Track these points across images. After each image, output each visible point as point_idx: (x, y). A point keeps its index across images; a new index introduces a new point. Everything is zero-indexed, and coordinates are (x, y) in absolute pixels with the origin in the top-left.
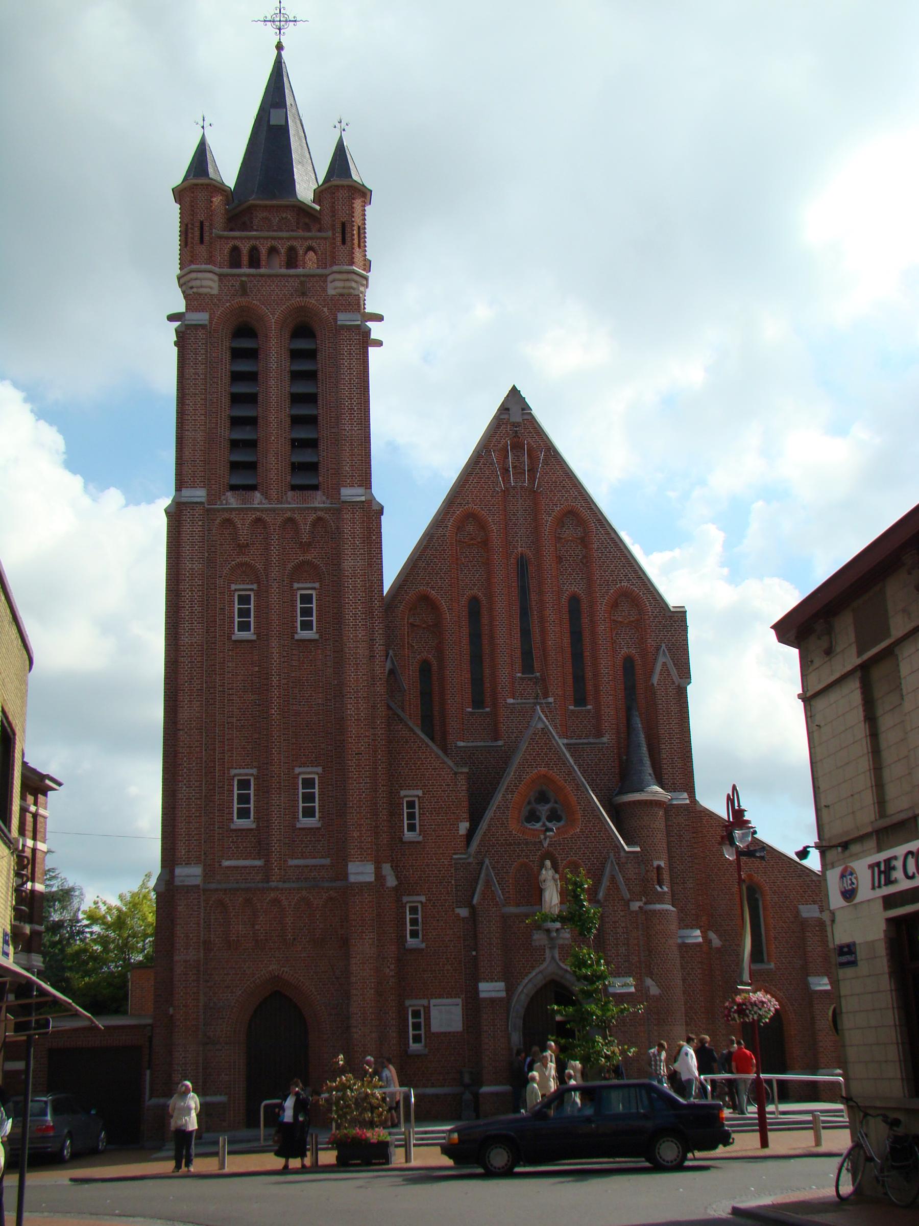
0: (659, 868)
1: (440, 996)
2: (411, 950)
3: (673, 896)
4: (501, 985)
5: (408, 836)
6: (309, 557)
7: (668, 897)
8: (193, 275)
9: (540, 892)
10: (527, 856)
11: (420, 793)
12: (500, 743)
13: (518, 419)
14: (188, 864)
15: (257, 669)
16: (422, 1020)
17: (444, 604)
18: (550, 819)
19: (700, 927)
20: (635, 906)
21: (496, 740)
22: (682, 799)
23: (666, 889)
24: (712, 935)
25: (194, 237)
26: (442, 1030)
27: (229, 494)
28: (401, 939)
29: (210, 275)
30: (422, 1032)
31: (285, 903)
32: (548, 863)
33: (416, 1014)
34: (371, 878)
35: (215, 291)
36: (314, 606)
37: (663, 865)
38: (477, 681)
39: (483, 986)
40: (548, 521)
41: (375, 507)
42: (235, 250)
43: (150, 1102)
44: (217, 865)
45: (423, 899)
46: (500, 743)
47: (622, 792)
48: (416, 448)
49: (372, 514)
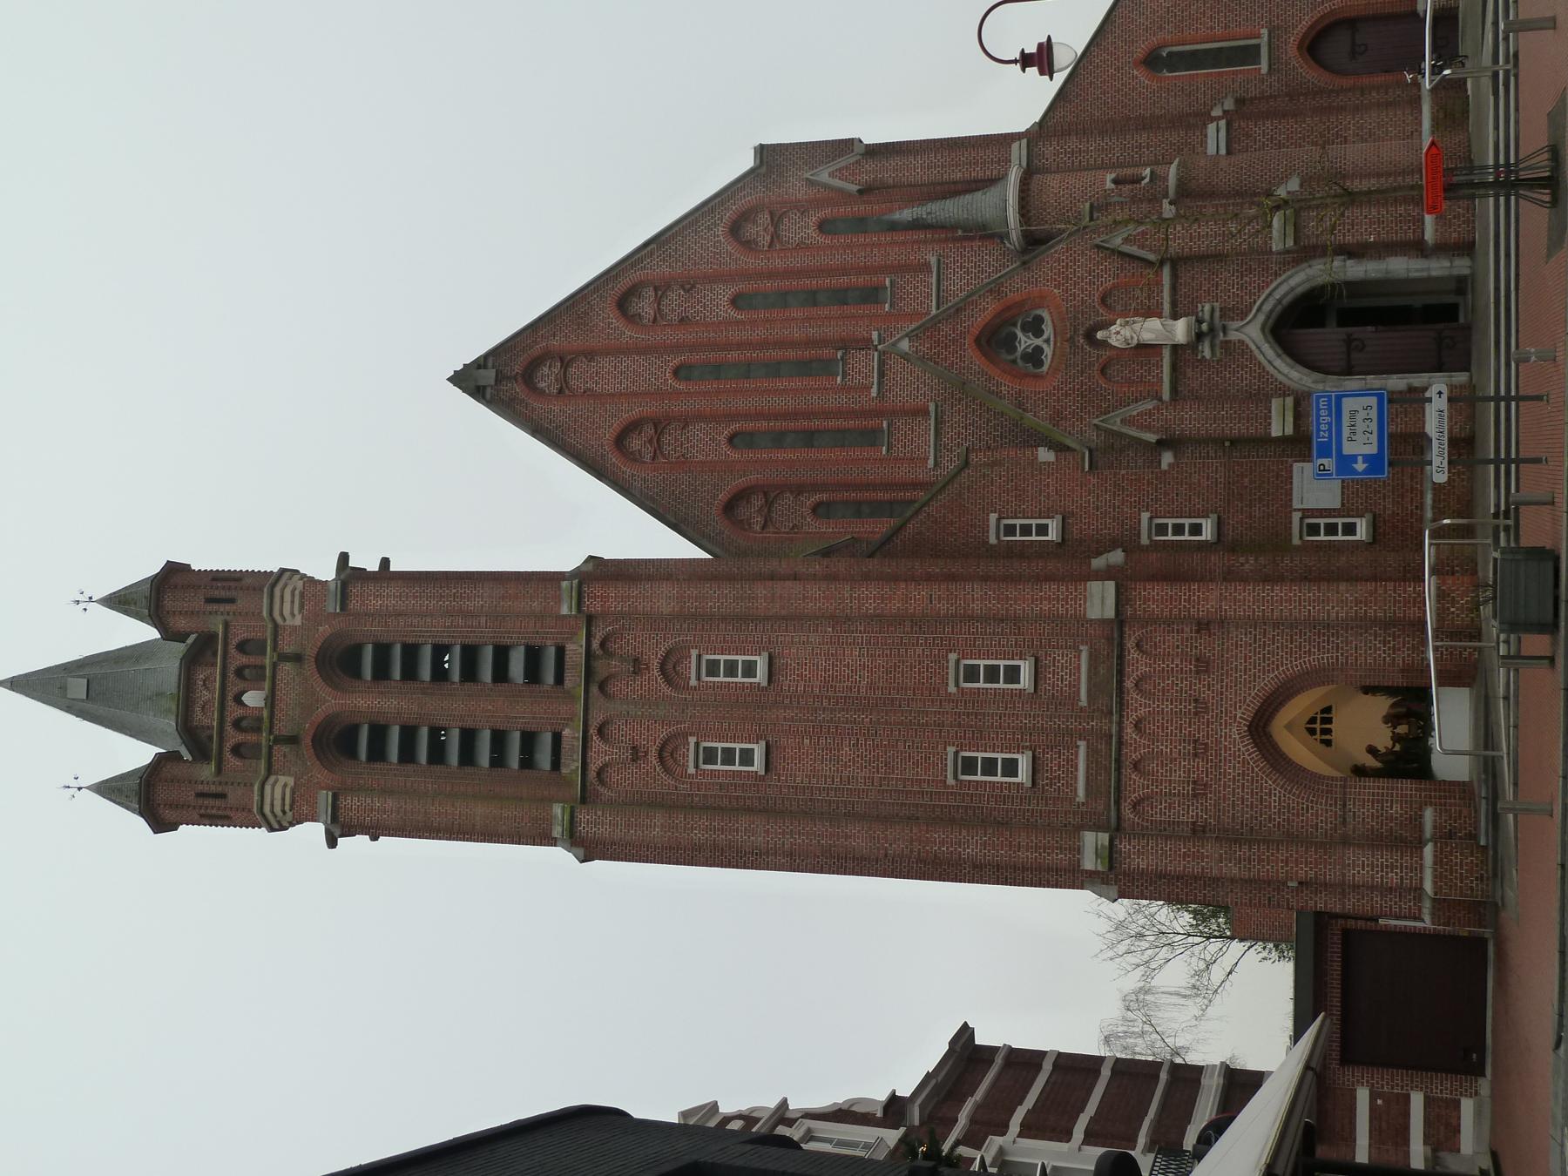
1: (1289, 493)
2: (1219, 535)
3: (1157, 163)
4: (1276, 404)
6: (655, 664)
7: (1159, 170)
8: (267, 809)
9: (1142, 347)
12: (932, 407)
13: (491, 373)
14: (1079, 851)
15: (807, 741)
16: (1322, 521)
17: (742, 482)
18: (1038, 333)
19: (1205, 125)
20: (1168, 210)
21: (927, 413)
22: (1018, 152)
23: (1148, 171)
25: (217, 809)
26: (1374, 438)
27: (564, 771)
28: (1201, 546)
29: (268, 788)
30: (1340, 521)
32: (1100, 335)
33: (1314, 529)
34: (1110, 586)
35: (291, 781)
38: (841, 438)
39: (1276, 432)
40: (629, 334)
41: (590, 567)
42: (237, 750)
43: (1427, 923)
44: (1084, 809)
45: (1145, 516)
46: (932, 407)
47: (1003, 237)
48: (547, 516)
49: (598, 572)
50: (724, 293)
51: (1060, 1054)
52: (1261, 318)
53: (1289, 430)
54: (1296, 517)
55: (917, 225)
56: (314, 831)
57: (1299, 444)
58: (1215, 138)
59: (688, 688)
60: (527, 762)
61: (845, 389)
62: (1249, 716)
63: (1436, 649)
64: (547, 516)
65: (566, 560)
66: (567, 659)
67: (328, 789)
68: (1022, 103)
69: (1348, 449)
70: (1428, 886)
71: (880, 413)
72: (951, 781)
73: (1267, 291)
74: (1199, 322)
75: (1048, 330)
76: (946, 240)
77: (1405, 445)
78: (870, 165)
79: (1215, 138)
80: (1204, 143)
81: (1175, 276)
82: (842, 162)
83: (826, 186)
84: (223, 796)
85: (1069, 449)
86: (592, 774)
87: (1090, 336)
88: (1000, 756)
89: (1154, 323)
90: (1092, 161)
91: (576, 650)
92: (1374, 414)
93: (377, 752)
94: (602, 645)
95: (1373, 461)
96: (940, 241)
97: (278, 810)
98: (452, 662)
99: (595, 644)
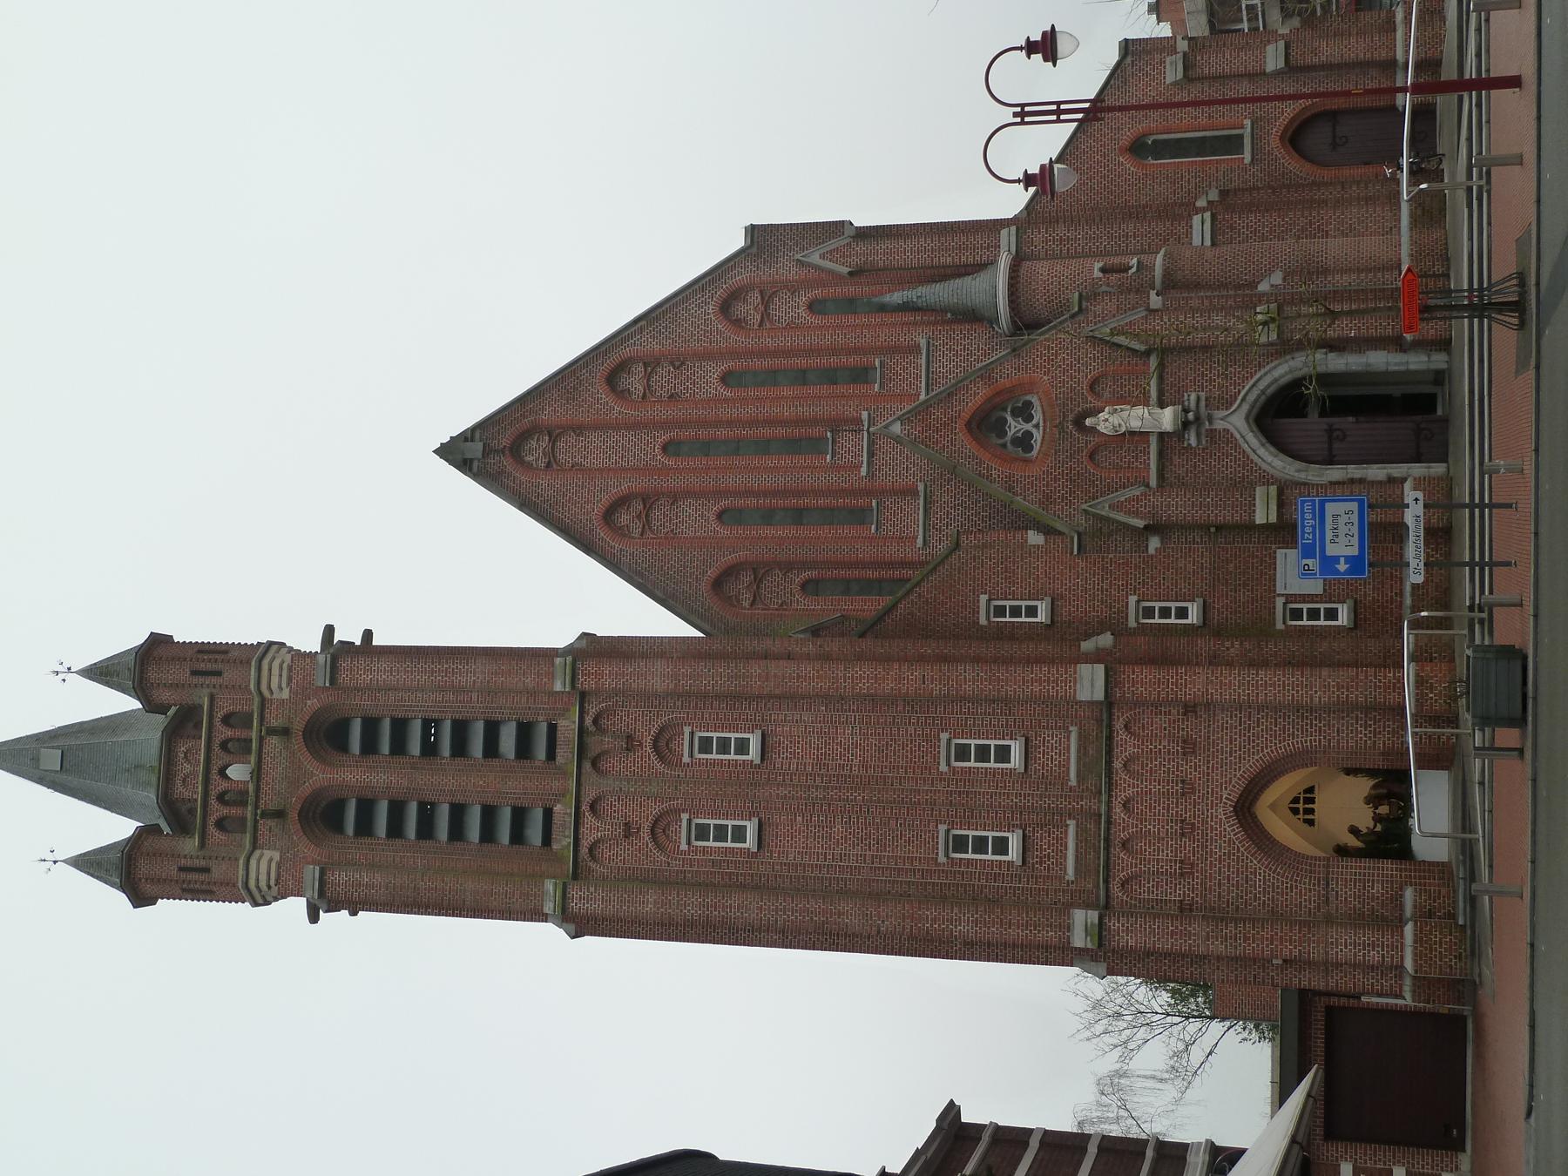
0: (1103, 270)
3: (1143, 252)
4: (1260, 492)
5: (1042, 617)
6: (648, 741)
10: (1080, 450)
11: (984, 598)
12: (921, 487)
16: (1305, 607)
17: (729, 559)
18: (1029, 419)
21: (915, 493)
22: (1007, 238)
23: (1135, 261)
24: (1201, 203)
25: (199, 884)
29: (253, 862)
30: (1322, 606)
31: (1130, 792)
32: (1088, 422)
33: (1297, 615)
35: (276, 856)
36: (715, 735)
37: (1101, 264)
38: (830, 516)
39: (1260, 519)
40: (618, 410)
42: (220, 824)
43: (1408, 1000)
46: (921, 487)
47: (993, 321)
48: (540, 591)
49: (591, 649)
50: (714, 371)
51: (1046, 1131)
52: (1246, 407)
53: (1273, 519)
54: (1280, 602)
55: (907, 307)
56: (296, 906)
57: (1284, 532)
58: (1200, 229)
59: (680, 764)
60: (518, 836)
61: (835, 468)
62: (1235, 797)
63: (1414, 734)
64: (540, 591)
65: (560, 637)
66: (559, 734)
67: (314, 863)
68: (1011, 202)
69: (1331, 550)
70: (1409, 964)
71: (869, 493)
72: (942, 859)
73: (1251, 382)
74: (1186, 411)
75: (1038, 416)
76: (935, 323)
77: (1384, 534)
78: (861, 247)
79: (1200, 229)
80: (1189, 234)
81: (1161, 366)
82: (833, 244)
83: (817, 268)
84: (207, 870)
85: (1060, 533)
86: (584, 851)
87: (1079, 422)
88: (990, 834)
89: (1139, 410)
90: (1079, 249)
91: (568, 727)
92: (1355, 518)
93: (365, 826)
94: (595, 721)
95: (1355, 563)
96: (929, 323)
97: (263, 884)
98: (508, 740)
99: (588, 721)
